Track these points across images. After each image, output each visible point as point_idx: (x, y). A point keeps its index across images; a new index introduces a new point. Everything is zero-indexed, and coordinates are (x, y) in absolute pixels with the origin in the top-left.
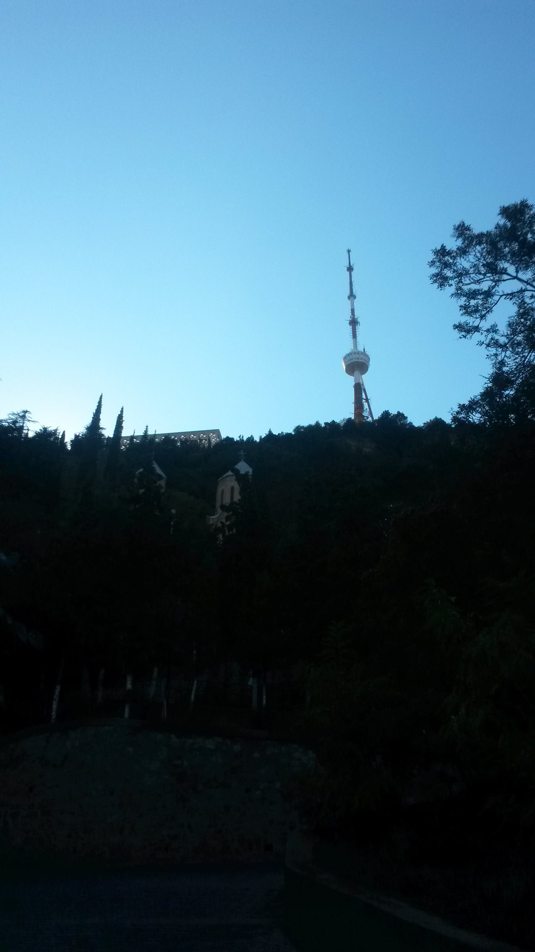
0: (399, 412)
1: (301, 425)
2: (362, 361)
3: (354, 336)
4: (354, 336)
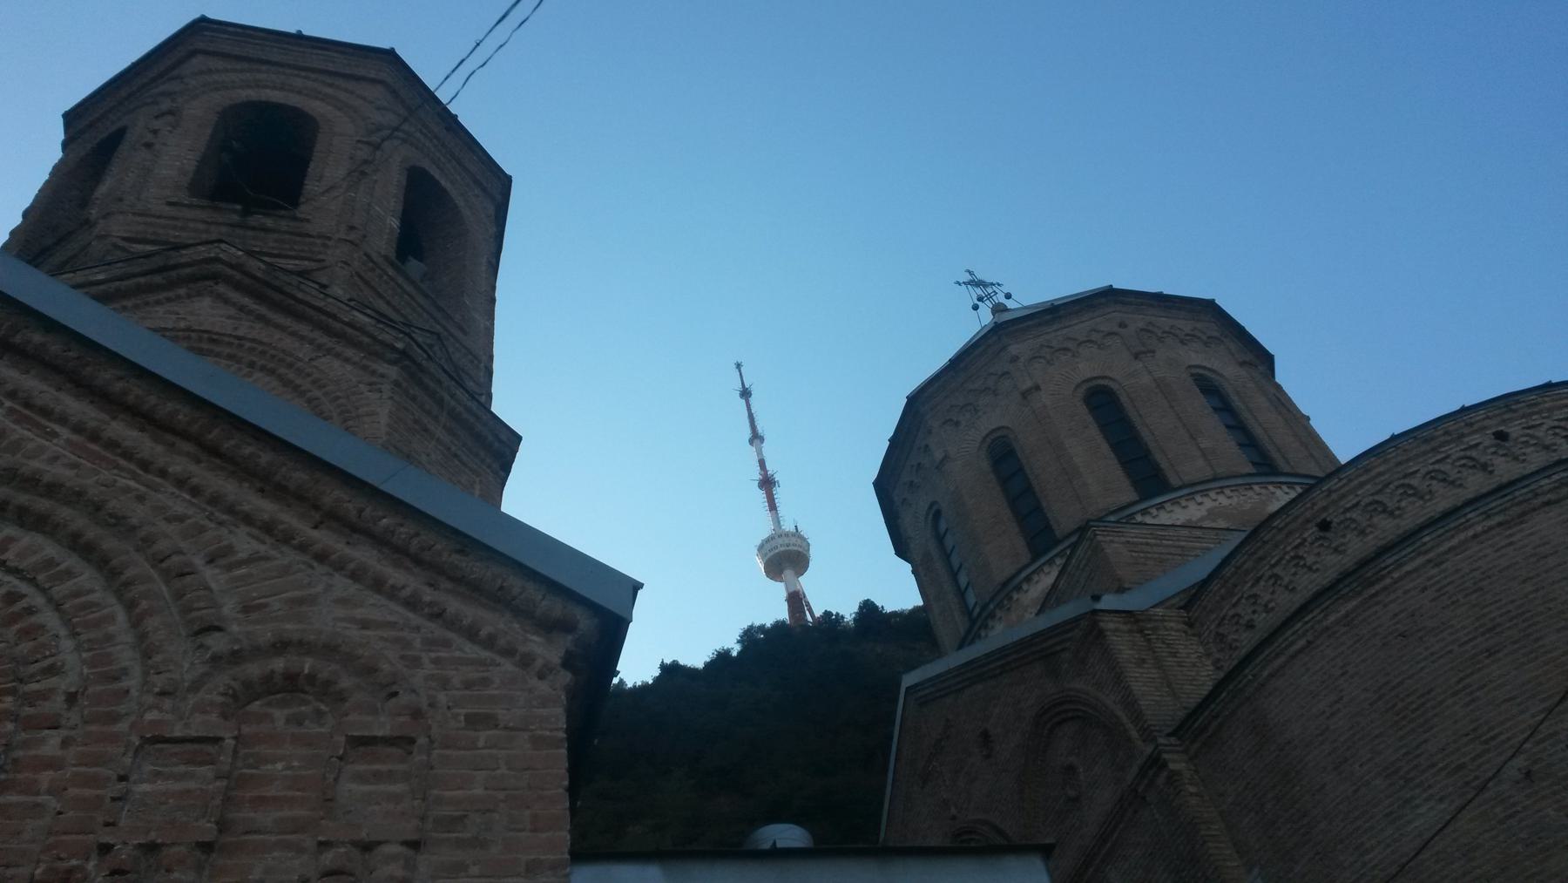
0: (663, 667)
1: (757, 624)
3: (772, 506)
4: (772, 506)
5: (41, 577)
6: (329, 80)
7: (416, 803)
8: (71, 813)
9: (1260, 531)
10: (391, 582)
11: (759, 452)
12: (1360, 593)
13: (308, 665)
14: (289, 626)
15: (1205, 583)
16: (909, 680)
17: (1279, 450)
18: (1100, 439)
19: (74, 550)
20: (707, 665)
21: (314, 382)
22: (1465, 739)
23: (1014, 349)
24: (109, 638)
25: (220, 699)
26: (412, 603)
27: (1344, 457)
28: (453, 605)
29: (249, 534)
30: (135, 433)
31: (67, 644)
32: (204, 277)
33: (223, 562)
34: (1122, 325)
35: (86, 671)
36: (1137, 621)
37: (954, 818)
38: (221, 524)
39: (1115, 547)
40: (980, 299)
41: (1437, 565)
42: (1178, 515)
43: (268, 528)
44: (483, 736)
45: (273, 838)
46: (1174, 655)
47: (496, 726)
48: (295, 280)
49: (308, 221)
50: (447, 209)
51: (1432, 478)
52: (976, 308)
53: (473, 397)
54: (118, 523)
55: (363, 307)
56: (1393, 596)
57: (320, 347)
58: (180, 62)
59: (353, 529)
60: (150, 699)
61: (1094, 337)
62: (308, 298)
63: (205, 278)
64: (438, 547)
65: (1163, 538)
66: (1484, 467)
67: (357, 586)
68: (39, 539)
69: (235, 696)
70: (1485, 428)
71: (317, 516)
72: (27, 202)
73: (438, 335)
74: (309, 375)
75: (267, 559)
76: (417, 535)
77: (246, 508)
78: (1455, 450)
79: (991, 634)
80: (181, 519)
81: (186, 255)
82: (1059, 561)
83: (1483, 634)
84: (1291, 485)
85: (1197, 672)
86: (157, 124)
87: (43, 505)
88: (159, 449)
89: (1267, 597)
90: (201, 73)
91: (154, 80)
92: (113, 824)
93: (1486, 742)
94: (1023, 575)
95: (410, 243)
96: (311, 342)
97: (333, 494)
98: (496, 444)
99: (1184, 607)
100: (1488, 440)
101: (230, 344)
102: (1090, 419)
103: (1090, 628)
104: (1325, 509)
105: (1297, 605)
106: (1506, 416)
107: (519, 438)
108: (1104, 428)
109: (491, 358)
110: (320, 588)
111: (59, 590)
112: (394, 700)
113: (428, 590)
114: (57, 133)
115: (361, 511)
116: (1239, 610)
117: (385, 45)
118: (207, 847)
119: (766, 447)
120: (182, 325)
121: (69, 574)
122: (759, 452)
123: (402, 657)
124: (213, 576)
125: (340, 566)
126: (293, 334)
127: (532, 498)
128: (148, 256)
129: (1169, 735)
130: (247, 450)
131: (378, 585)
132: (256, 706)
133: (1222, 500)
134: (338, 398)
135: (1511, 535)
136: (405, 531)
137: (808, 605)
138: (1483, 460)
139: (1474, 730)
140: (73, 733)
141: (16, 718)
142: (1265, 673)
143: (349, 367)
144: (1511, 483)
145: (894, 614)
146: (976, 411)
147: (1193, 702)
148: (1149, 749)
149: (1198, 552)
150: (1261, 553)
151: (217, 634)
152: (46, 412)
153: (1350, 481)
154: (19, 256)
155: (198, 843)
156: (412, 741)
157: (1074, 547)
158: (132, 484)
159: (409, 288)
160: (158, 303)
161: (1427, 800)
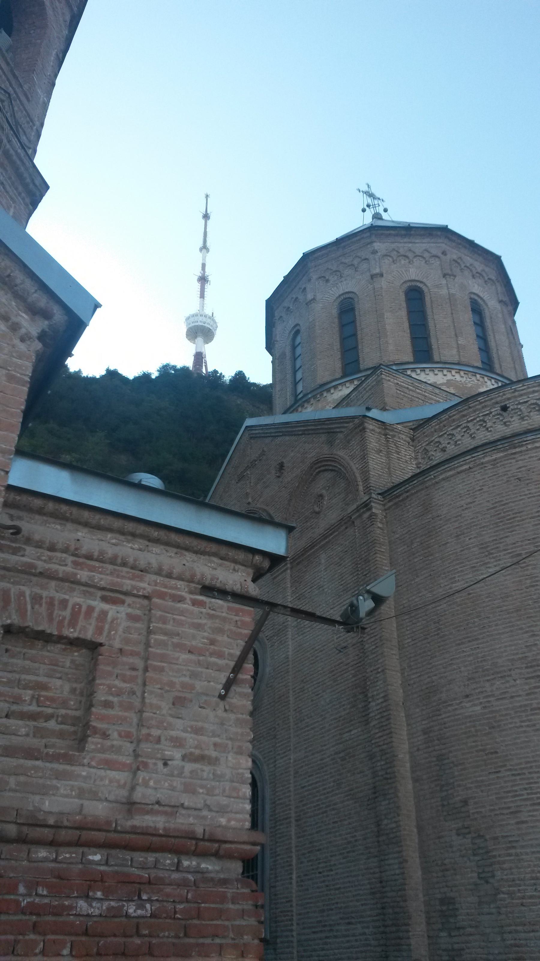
0: (108, 371)
1: (172, 363)
2: (209, 326)
3: (202, 296)
4: (202, 296)
9: (468, 400)
11: (204, 258)
16: (249, 422)
17: (499, 359)
20: (136, 379)
23: (377, 245)
27: (531, 373)
36: (386, 429)
37: (249, 503)
39: (390, 384)
40: (368, 206)
42: (431, 378)
46: (398, 453)
52: (364, 210)
56: (522, 458)
61: (426, 255)
65: (417, 388)
73: (9, 94)
79: (304, 411)
82: (356, 383)
84: (497, 381)
85: (406, 465)
89: (459, 437)
98: (31, 186)
102: (404, 305)
103: (359, 424)
104: (509, 399)
105: (472, 447)
109: (42, 125)
116: (441, 440)
119: (209, 256)
122: (204, 258)
127: (49, 229)
129: (379, 494)
133: (458, 377)
139: (534, 539)
142: (441, 477)
145: (254, 384)
146: (341, 277)
147: (397, 481)
148: (366, 498)
149: (433, 402)
153: (529, 388)
157: (367, 377)
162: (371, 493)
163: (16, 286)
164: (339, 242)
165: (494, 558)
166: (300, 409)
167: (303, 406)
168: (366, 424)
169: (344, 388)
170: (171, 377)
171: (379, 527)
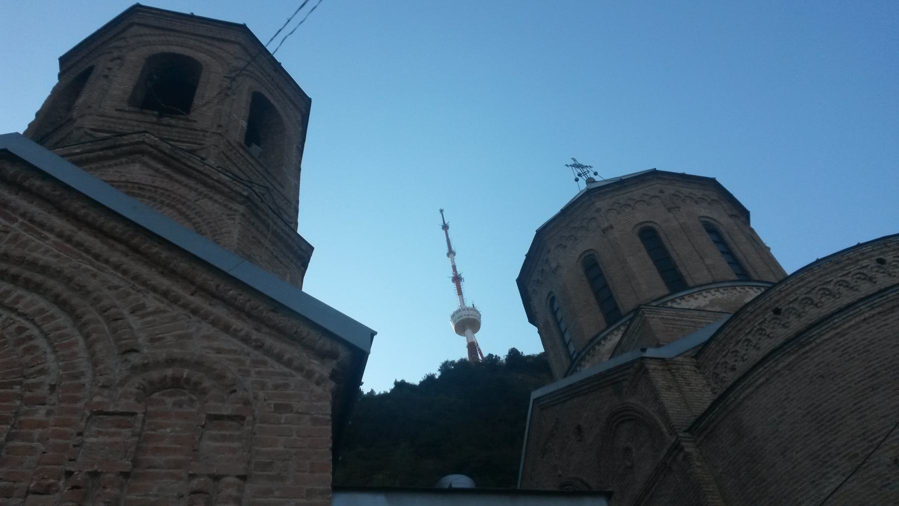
0: (396, 383)
1: (450, 360)
5: (37, 319)
6: (208, 41)
7: (245, 454)
8: (51, 453)
9: (739, 314)
10: (234, 327)
11: (453, 261)
12: (797, 351)
13: (186, 373)
14: (176, 351)
15: (706, 344)
16: (535, 394)
18: (647, 257)
19: (56, 304)
20: (421, 383)
21: (196, 213)
22: (858, 439)
23: (598, 204)
24: (74, 354)
25: (135, 391)
26: (246, 340)
27: (789, 269)
28: (269, 341)
29: (155, 297)
30: (91, 239)
31: (51, 357)
32: (135, 152)
33: (140, 313)
34: (661, 192)
35: (61, 372)
36: (667, 364)
37: (560, 476)
38: (139, 291)
39: (656, 321)
40: (580, 175)
41: (843, 336)
42: (693, 303)
43: (165, 294)
44: (284, 417)
45: (164, 471)
46: (688, 384)
47: (291, 411)
48: (187, 155)
49: (195, 121)
50: (275, 117)
51: (840, 285)
52: (577, 180)
53: (286, 224)
54: (82, 291)
55: (226, 171)
57: (200, 193)
58: (124, 30)
59: (214, 296)
60: (96, 390)
61: (646, 198)
62: (194, 166)
63: (137, 153)
64: (261, 308)
66: (871, 279)
67: (215, 329)
68: (36, 297)
69: (144, 390)
70: (871, 256)
71: (193, 288)
72: (38, 107)
74: (194, 209)
75: (164, 312)
76: (249, 300)
77: (154, 282)
78: (853, 269)
80: (116, 288)
81: (126, 140)
82: (623, 328)
83: (869, 377)
84: (758, 287)
85: (703, 396)
86: (110, 65)
87: (39, 278)
88: (105, 248)
89: (744, 352)
90: (137, 36)
91: (111, 39)
92: (74, 460)
93: (871, 441)
94: (602, 335)
95: (253, 136)
96: (196, 190)
97: (202, 276)
98: (300, 252)
99: (695, 357)
100: (873, 264)
101: (150, 190)
102: (642, 246)
103: (639, 367)
104: (777, 301)
106: (885, 249)
107: (312, 249)
108: (650, 251)
109: (298, 202)
110: (193, 330)
111: (46, 327)
112: (233, 395)
113: (255, 332)
114: (56, 69)
115: (218, 286)
117: (241, 22)
118: (126, 475)
120: (123, 179)
121: (52, 317)
122: (453, 261)
123: (240, 370)
124: (134, 321)
125: (205, 317)
126: (186, 186)
127: (321, 283)
128: (104, 139)
129: (685, 431)
130: (155, 250)
131: (226, 329)
132: (156, 395)
133: (719, 295)
134: (210, 223)
135: (886, 320)
136: (242, 298)
137: (479, 350)
138: (870, 275)
139: (864, 434)
140: (52, 408)
141: (20, 397)
143: (217, 205)
144: (886, 289)
145: (529, 357)
147: (699, 412)
148: (673, 441)
150: (740, 326)
151: (135, 354)
152: (42, 225)
154: (33, 138)
155: (121, 473)
156: (243, 418)
157: (631, 320)
158: (90, 267)
159: (252, 161)
160: (110, 166)
161: (836, 474)
162: (676, 433)
163: (303, 338)
164: (564, 212)
165: (830, 466)
166: (578, 369)
167: (580, 365)
168: (647, 366)
169: (613, 337)
170: (452, 372)
171: (698, 466)
